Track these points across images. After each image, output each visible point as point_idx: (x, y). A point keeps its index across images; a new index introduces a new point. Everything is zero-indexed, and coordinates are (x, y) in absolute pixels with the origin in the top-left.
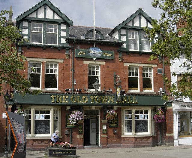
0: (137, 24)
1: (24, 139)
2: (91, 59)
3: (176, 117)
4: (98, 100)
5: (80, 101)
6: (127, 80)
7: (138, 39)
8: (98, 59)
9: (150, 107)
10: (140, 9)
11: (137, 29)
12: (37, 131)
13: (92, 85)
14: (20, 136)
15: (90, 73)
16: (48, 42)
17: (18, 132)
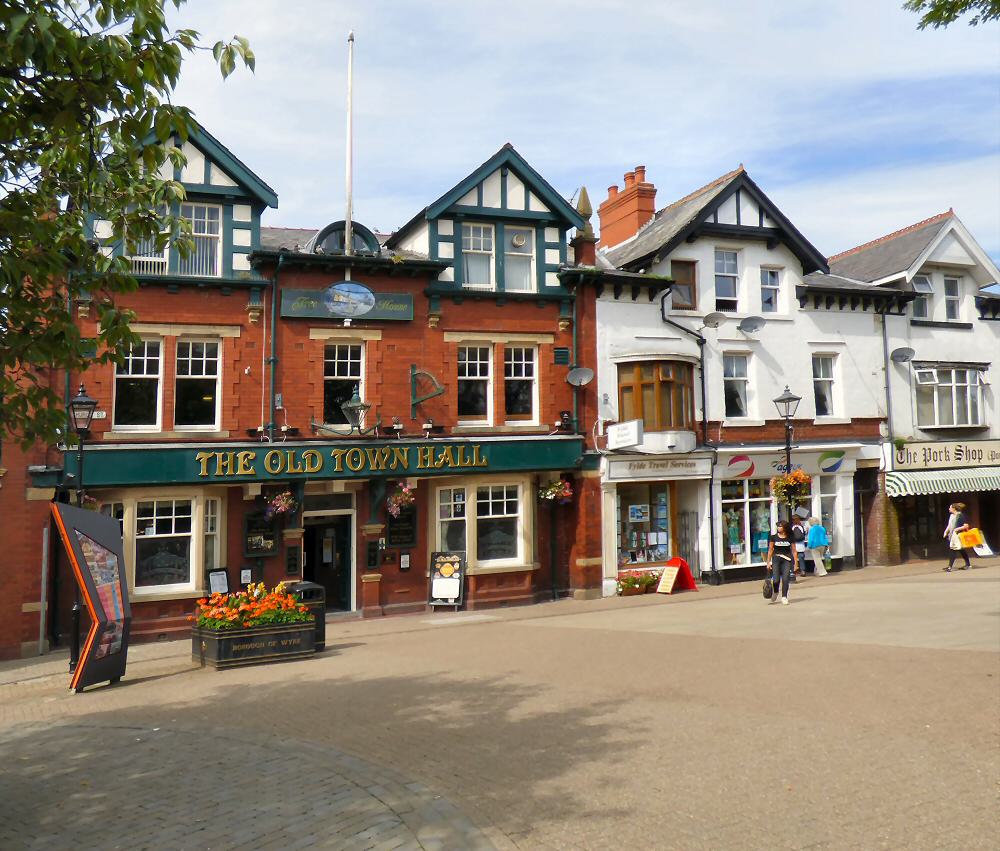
0: (492, 200)
1: (120, 606)
2: (336, 322)
3: (609, 506)
4: (277, 465)
5: (295, 467)
6: (454, 391)
7: (493, 252)
8: (359, 323)
9: (528, 474)
10: (508, 148)
11: (728, 234)
12: (145, 574)
13: (337, 407)
14: (108, 595)
15: (329, 370)
16: (185, 269)
17: (98, 579)
